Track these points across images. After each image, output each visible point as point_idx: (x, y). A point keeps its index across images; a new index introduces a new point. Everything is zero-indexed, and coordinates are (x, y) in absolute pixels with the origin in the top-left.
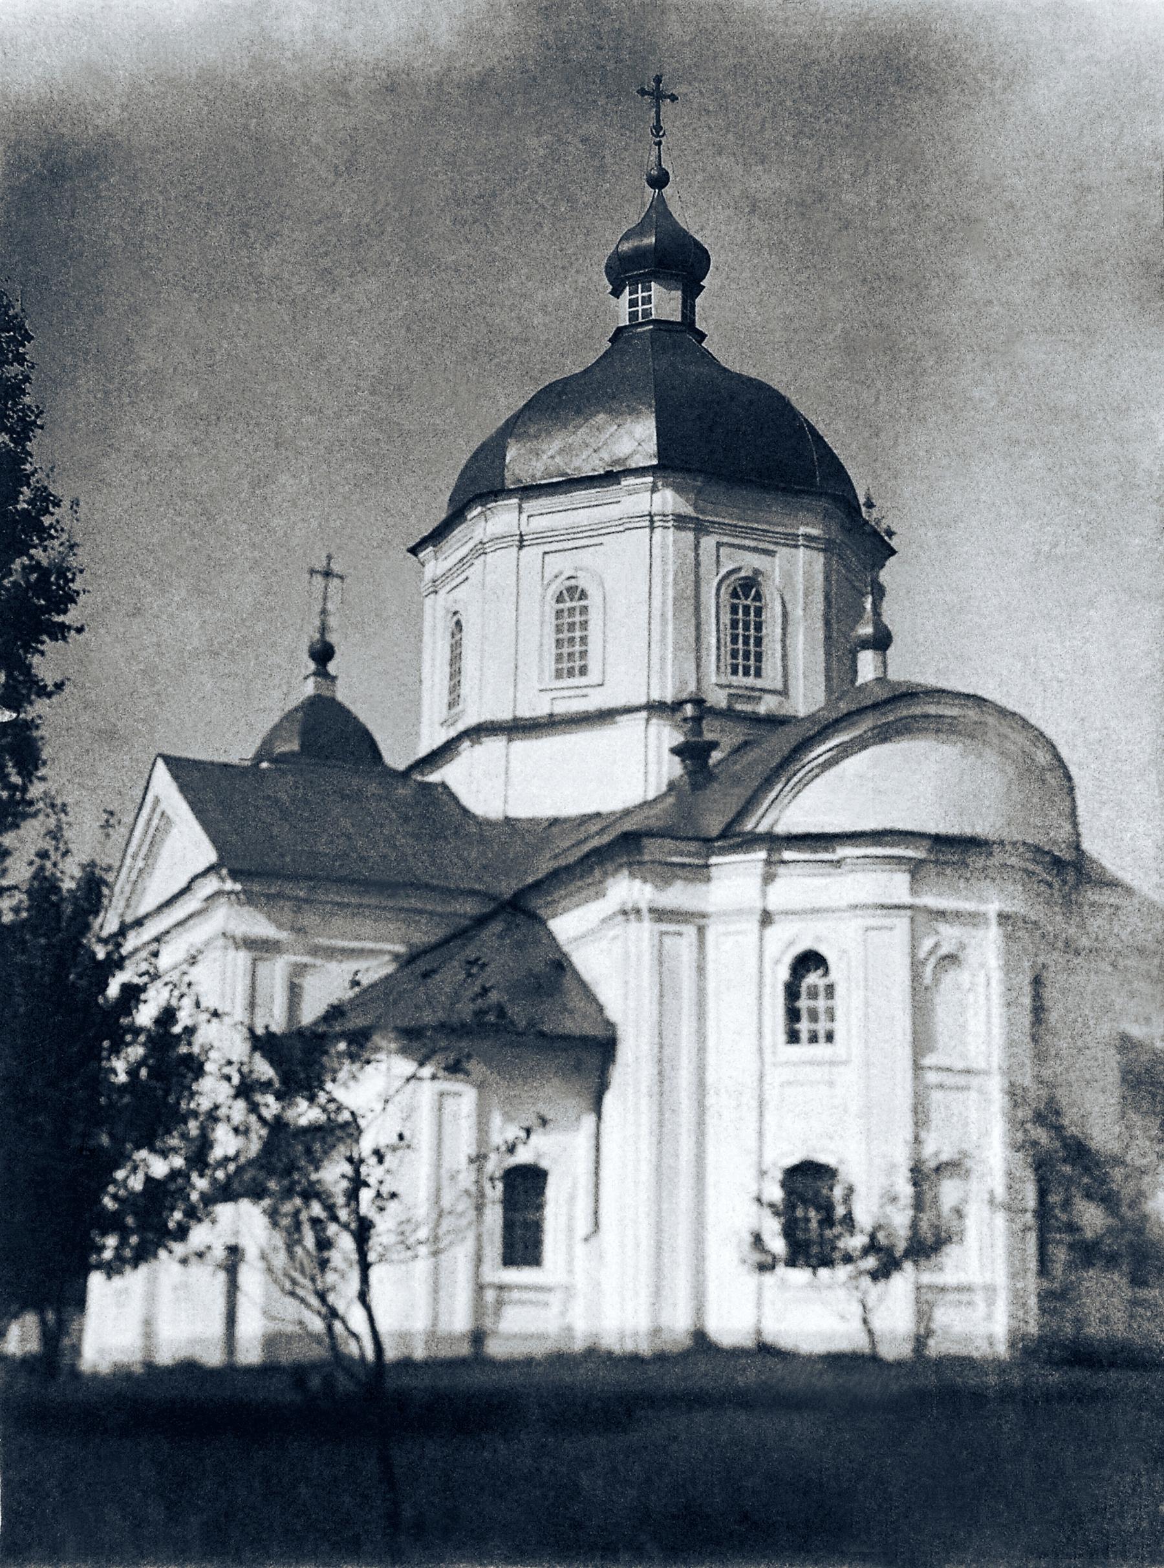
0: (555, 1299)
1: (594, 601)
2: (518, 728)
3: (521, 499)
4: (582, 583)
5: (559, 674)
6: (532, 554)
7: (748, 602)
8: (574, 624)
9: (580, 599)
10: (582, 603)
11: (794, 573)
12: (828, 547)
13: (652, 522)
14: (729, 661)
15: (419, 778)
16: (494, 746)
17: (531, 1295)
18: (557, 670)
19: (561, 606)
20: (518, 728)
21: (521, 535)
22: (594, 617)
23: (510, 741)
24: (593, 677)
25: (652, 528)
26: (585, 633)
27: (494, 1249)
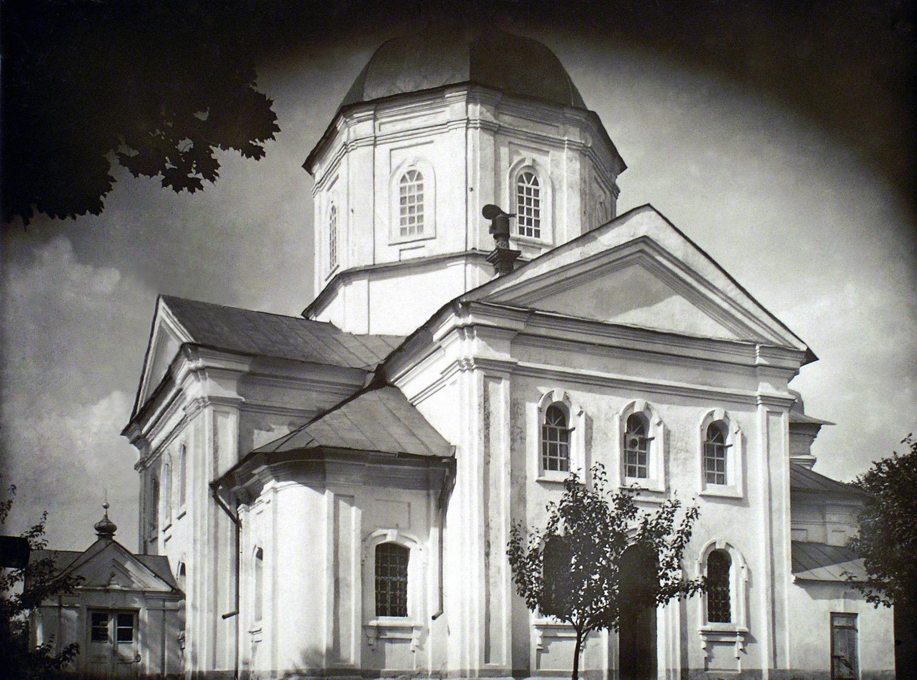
0: (415, 634)
1: (427, 181)
2: (375, 271)
3: (375, 111)
4: (418, 168)
5: (403, 231)
6: (382, 151)
7: (530, 186)
8: (413, 207)
9: (417, 179)
10: (419, 182)
11: (561, 171)
12: (583, 152)
13: (467, 124)
14: (518, 225)
15: (314, 319)
16: (359, 286)
17: (398, 635)
18: (402, 229)
19: (403, 185)
20: (375, 271)
21: (375, 137)
22: (428, 193)
23: (369, 281)
24: (428, 232)
25: (467, 128)
26: (421, 193)
27: (372, 605)
